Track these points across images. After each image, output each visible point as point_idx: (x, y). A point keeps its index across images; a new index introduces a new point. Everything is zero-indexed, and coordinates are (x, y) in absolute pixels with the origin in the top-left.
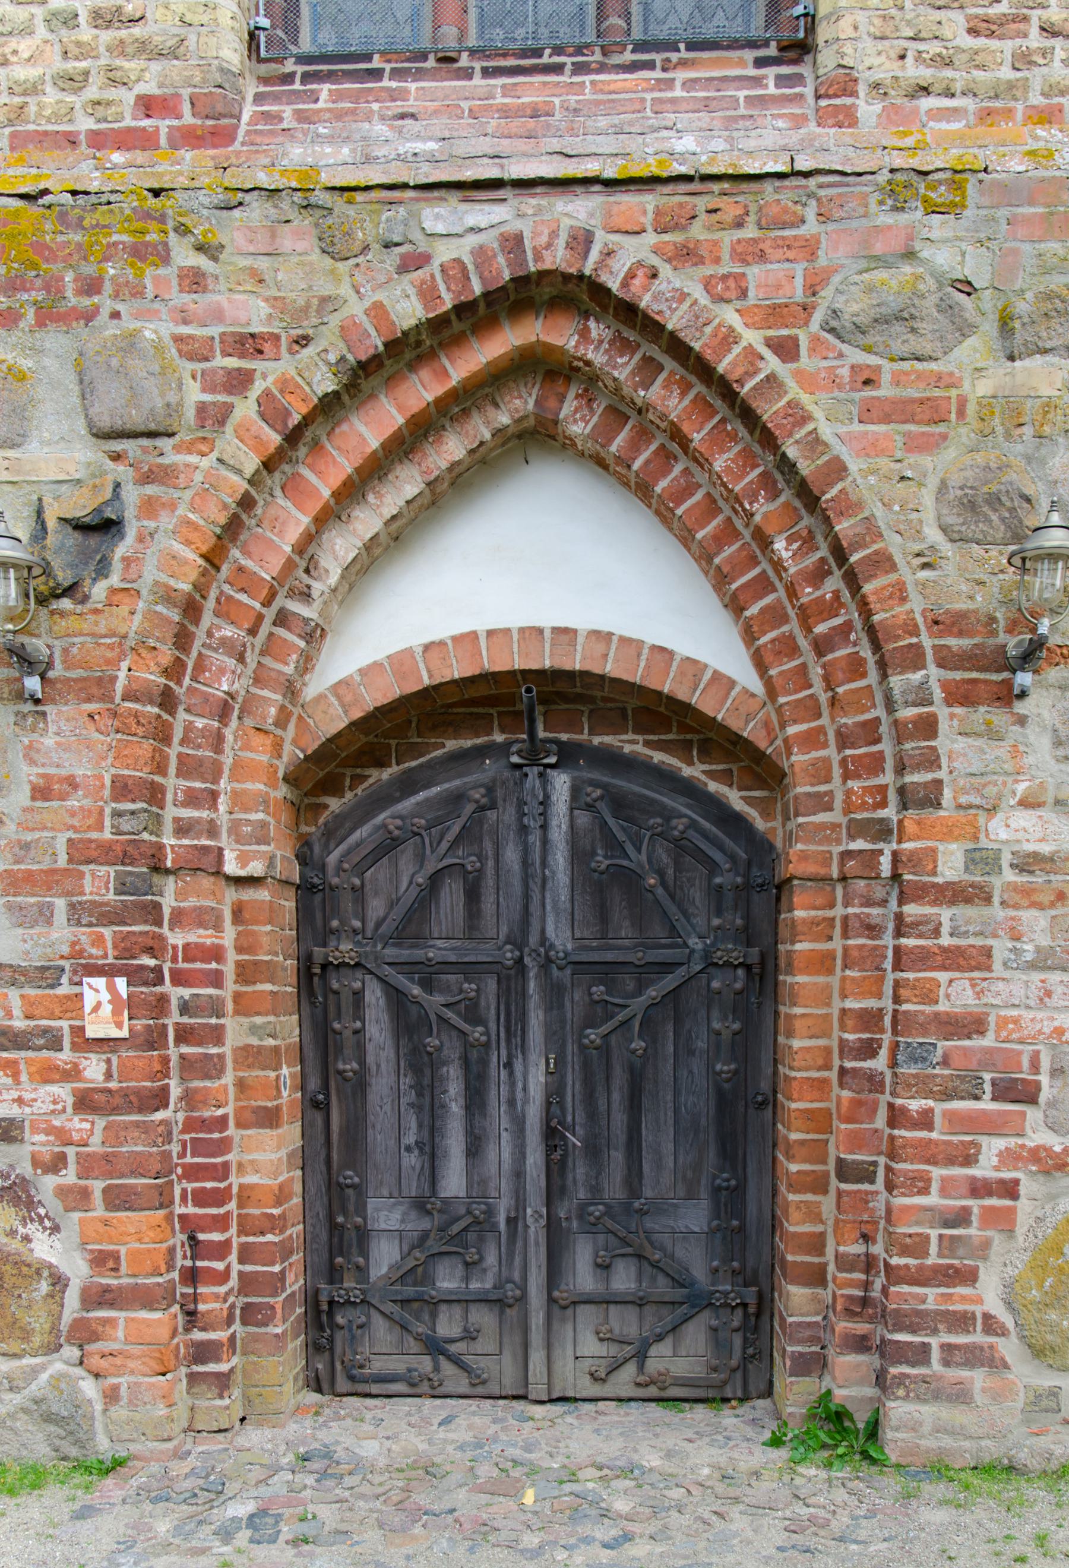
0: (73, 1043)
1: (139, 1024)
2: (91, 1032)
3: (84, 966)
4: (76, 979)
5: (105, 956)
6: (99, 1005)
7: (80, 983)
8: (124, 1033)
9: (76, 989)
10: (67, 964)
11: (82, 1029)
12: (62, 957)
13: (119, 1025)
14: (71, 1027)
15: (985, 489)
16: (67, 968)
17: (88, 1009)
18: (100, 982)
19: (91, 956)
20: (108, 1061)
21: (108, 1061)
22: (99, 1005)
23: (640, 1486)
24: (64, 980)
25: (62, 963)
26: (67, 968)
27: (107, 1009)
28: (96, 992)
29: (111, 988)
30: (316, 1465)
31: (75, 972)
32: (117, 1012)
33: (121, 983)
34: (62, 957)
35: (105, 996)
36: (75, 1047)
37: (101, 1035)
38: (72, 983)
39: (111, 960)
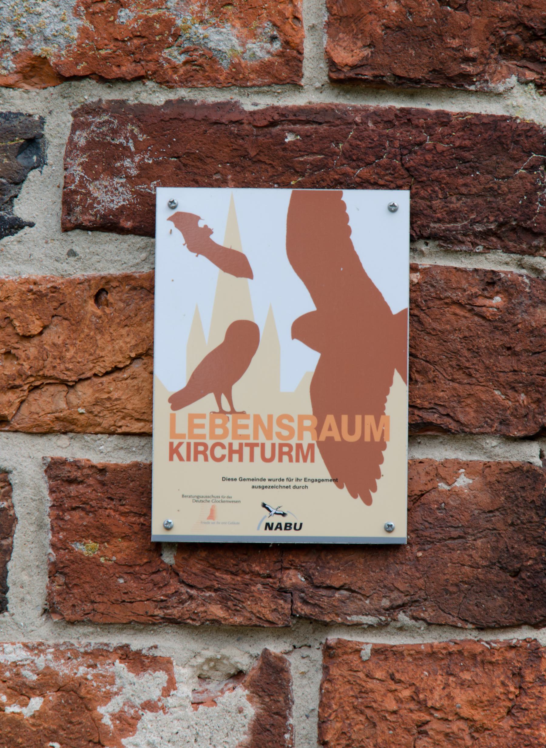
0: (63, 570)
1: (467, 465)
2: (189, 503)
3: (160, 124)
4: (110, 195)
5: (286, 70)
6: (242, 341)
7: (141, 224)
8: (381, 515)
9: (109, 256)
10: (53, 112)
11: (136, 486)
12: (35, 70)
13: (355, 470)
14: (58, 473)
15: (68, 278)
16: (58, 129)
17: (171, 369)
18: (255, 216)
19: (202, 67)
20: (270, 683)
21: (270, 683)
22: (242, 341)
23: (87, 336)
24: (37, 200)
25: (27, 101)
26: (58, 129)
27: (287, 371)
28: (225, 270)
29: (321, 252)
30: (212, 664)
31: (102, 156)
32: (339, 391)
33: (378, 225)
34: (35, 70)
35: (280, 296)
36: (73, 594)
37: (243, 523)
38: (78, 217)
39: (311, 95)
